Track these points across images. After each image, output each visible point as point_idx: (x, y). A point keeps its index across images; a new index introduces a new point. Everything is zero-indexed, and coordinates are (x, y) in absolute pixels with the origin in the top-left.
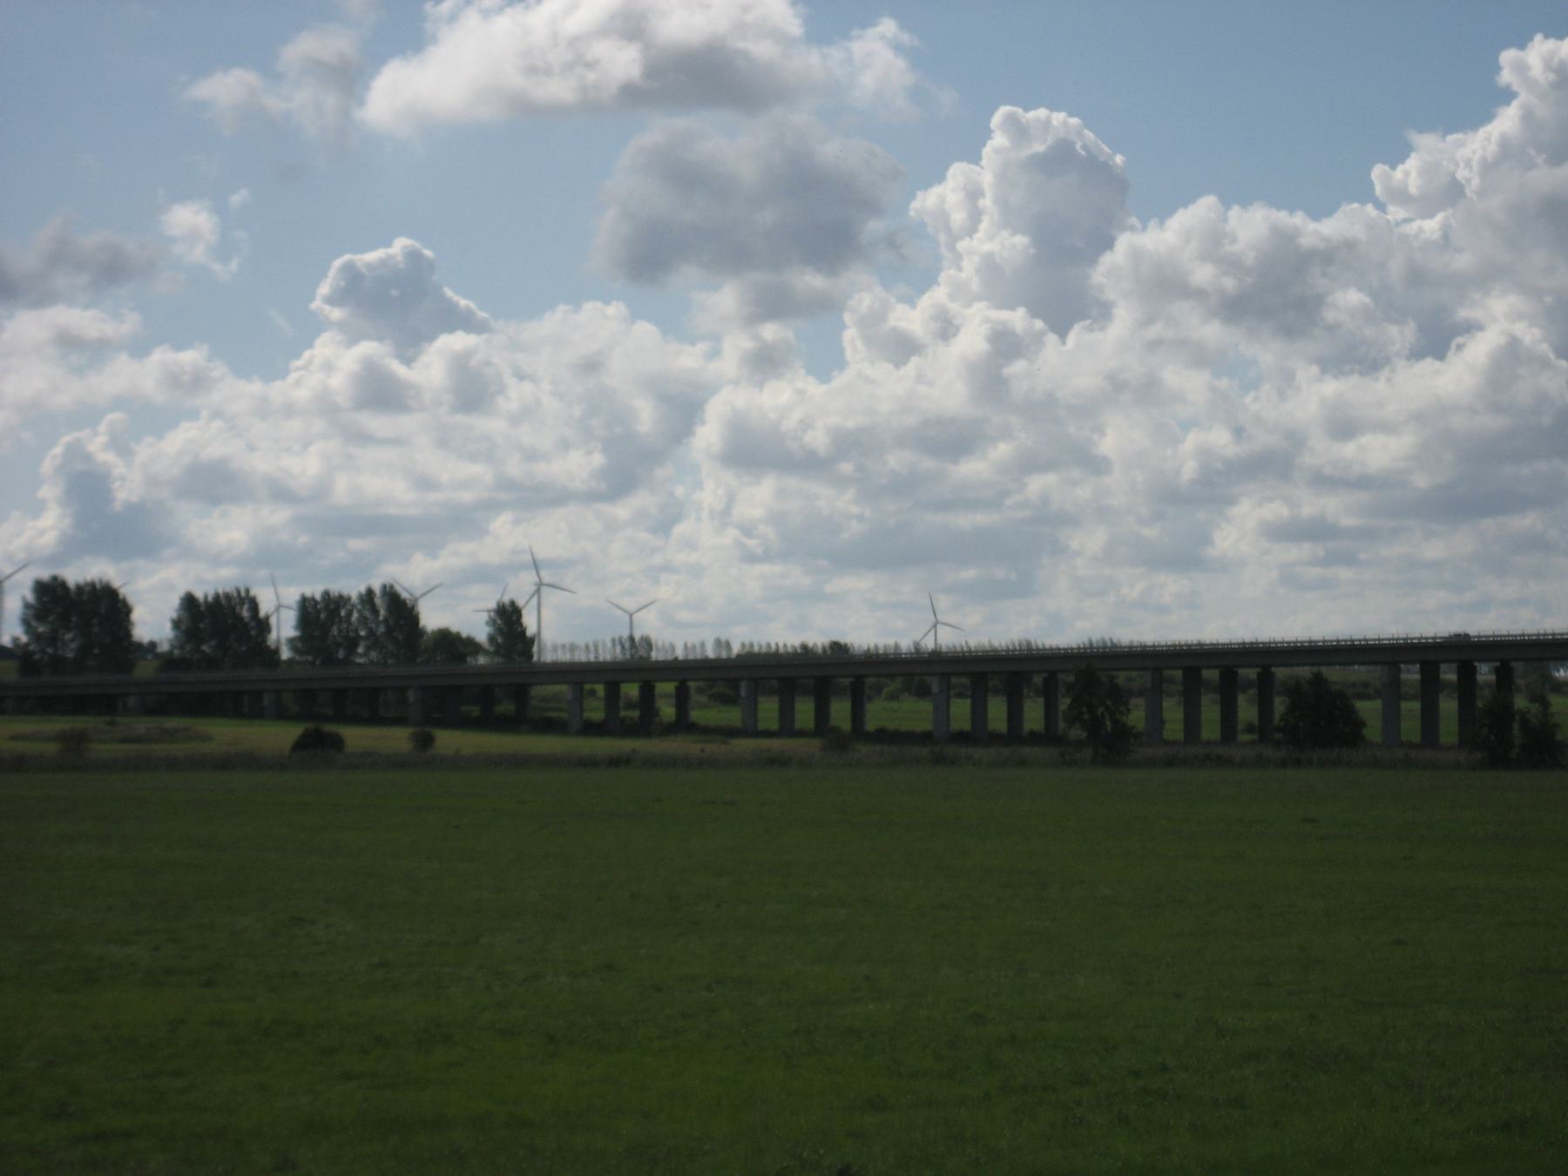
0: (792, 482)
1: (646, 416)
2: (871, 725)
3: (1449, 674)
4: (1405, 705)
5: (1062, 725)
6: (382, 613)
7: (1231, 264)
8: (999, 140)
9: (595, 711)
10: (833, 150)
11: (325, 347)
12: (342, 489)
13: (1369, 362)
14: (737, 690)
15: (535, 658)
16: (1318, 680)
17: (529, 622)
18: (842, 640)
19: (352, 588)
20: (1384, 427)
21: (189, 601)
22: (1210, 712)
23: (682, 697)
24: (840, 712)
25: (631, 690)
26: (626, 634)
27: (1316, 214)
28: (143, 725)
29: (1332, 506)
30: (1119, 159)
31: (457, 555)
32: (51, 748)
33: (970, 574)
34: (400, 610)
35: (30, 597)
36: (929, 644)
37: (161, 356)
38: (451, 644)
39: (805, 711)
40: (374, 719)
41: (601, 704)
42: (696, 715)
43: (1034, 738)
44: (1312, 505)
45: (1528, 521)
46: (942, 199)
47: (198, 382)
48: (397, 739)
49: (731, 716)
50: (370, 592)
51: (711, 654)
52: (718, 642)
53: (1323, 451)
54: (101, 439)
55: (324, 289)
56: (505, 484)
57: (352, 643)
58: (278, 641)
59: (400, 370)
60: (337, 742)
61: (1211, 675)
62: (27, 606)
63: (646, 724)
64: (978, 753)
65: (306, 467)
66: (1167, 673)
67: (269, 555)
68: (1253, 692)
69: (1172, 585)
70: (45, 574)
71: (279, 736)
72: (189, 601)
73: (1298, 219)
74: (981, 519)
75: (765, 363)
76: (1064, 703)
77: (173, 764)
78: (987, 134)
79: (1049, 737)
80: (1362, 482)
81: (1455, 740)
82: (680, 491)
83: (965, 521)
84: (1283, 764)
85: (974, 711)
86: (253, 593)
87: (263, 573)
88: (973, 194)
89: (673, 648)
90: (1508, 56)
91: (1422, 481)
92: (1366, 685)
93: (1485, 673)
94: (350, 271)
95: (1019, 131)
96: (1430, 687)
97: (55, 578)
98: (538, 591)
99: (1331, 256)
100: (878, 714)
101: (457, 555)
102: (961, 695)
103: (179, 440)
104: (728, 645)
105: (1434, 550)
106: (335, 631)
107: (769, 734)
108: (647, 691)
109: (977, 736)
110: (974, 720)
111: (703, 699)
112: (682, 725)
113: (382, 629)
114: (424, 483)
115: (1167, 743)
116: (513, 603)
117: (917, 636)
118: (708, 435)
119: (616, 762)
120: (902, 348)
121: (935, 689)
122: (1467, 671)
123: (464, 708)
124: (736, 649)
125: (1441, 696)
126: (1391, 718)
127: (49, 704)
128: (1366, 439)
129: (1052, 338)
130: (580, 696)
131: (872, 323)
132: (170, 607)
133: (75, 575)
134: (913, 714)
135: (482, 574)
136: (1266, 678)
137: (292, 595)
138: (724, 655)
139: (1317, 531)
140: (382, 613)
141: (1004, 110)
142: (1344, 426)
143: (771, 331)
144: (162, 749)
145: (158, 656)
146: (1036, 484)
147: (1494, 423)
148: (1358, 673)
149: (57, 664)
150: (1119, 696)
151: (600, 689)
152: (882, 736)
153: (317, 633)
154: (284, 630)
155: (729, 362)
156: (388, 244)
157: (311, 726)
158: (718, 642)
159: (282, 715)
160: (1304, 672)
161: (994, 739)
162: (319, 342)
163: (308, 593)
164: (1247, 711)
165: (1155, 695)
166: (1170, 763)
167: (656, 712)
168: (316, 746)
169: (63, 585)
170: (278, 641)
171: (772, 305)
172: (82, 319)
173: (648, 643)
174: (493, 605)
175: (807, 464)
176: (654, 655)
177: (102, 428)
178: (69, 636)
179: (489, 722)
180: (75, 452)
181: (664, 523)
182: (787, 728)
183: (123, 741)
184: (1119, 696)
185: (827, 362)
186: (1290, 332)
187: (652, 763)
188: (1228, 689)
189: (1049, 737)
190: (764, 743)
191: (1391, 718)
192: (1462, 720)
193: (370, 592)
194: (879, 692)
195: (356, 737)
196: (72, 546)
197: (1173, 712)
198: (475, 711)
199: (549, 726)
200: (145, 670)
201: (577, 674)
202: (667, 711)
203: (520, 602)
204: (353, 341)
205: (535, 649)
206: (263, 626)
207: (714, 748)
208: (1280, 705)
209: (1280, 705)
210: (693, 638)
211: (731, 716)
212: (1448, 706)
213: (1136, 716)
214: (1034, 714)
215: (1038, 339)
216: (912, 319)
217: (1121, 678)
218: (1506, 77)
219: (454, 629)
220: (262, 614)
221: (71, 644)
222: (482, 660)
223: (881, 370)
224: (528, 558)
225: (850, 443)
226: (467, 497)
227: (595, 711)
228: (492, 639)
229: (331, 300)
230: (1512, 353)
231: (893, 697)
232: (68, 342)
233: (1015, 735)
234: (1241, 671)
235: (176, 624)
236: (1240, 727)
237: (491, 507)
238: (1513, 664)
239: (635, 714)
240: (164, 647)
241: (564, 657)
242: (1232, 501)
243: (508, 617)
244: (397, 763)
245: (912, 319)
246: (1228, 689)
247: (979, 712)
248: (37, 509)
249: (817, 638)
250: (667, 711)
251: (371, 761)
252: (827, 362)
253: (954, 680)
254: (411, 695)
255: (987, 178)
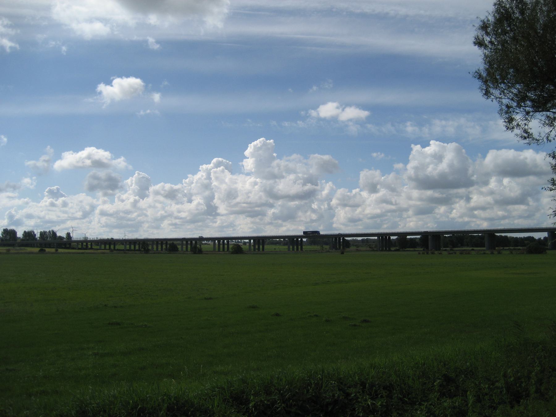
0: (109, 218)
1: (88, 208)
2: (116, 249)
3: (189, 242)
4: (184, 246)
5: (141, 248)
6: (51, 233)
7: (165, 190)
8: (136, 174)
9: (80, 247)
10: (114, 175)
11: (45, 199)
12: (47, 217)
13: (182, 203)
14: (99, 244)
15: (72, 240)
16: (173, 243)
17: (71, 235)
18: (113, 238)
19: (47, 230)
20: (185, 212)
21: (25, 232)
22: (160, 247)
23: (91, 245)
24: (112, 247)
25: (85, 244)
26: (84, 237)
27: (176, 185)
28: (18, 248)
29: (177, 221)
30: (149, 177)
31: (62, 226)
32: (5, 251)
33: (130, 229)
34: (54, 234)
35: (3, 231)
36: (124, 238)
37: (22, 199)
38: (61, 238)
39: (107, 247)
40: (50, 247)
41: (81, 246)
42: (93, 247)
43: (137, 250)
44: (175, 221)
45: (200, 224)
46: (128, 181)
47: (27, 203)
48: (53, 250)
49: (98, 247)
50: (50, 231)
51: (96, 239)
52: (96, 238)
53: (176, 214)
54: (13, 210)
55: (47, 190)
56: (69, 217)
57: (47, 238)
58: (37, 237)
59: (56, 202)
60: (45, 250)
61: (160, 242)
62: (2, 232)
63: (87, 248)
64: (130, 252)
65: (42, 214)
66: (154, 242)
67: (37, 226)
68: (165, 244)
69: (155, 231)
70: (5, 228)
71: (37, 250)
72: (25, 232)
73: (173, 186)
74: (132, 222)
75: (104, 202)
76: (141, 246)
77: (22, 253)
78: (135, 174)
79: (139, 250)
80: (181, 218)
81: (190, 250)
82: (92, 218)
83: (130, 223)
84: (168, 253)
85: (109, 247)
86: (34, 231)
87: (35, 228)
88: (132, 181)
89: (91, 238)
90: (201, 166)
91: (188, 218)
92: (179, 244)
93: (194, 242)
94: (50, 189)
95: (139, 174)
96: (187, 244)
97: (6, 229)
98: (73, 231)
99: (177, 191)
100: (117, 247)
101: (62, 226)
102: (128, 245)
103: (24, 211)
104: (98, 238)
105: (189, 227)
106: (45, 236)
107: (103, 250)
108: (87, 244)
109: (130, 250)
110: (129, 248)
111: (94, 245)
112: (91, 248)
113: (51, 236)
114: (59, 217)
115: (154, 251)
116: (69, 233)
117: (122, 237)
118: (97, 211)
119: (83, 253)
120: (123, 201)
121: (125, 244)
122: (191, 242)
123: (62, 246)
124: (99, 239)
125: (188, 245)
126: (182, 247)
127: (4, 245)
128: (182, 213)
129: (141, 200)
130: (78, 244)
131: (119, 198)
132: (22, 233)
133: (9, 228)
134: (122, 247)
135: (66, 229)
136: (167, 243)
137: (39, 231)
138: (97, 239)
139: (175, 224)
140: (51, 233)
141: (137, 172)
142: (179, 211)
143: (106, 198)
144: (20, 251)
145: (21, 239)
146: (139, 218)
147: (196, 212)
148: (178, 242)
149: (6, 240)
150: (148, 245)
151: (81, 244)
152: (118, 250)
153: (43, 236)
154: (38, 236)
155: (100, 202)
156: (54, 187)
157: (41, 248)
158: (96, 238)
159: (37, 247)
160: (171, 242)
161: (132, 250)
162: (44, 198)
163: (41, 231)
164: (164, 247)
165: (153, 245)
166: (154, 253)
167: (88, 247)
168: (42, 251)
169: (8, 230)
170: (421, 199)
171: (105, 195)
172: (11, 194)
173: (87, 238)
174: (67, 233)
175: (111, 215)
176: (88, 239)
177: (14, 209)
178: (8, 236)
179: (66, 248)
180: (10, 213)
181: (90, 222)
182: (105, 249)
183: (15, 250)
184: (148, 245)
185: (112, 202)
186: (172, 200)
187: (87, 253)
188: (162, 244)
189: (139, 250)
190: (102, 251)
191: (182, 247)
192: (191, 248)
193: (50, 231)
194: (117, 244)
195: (47, 250)
196: (9, 225)
197: (155, 247)
198: (64, 246)
199: (73, 248)
200: (19, 241)
201: (78, 242)
202: (89, 247)
203: (70, 233)
204: (49, 198)
205: (72, 239)
206: (35, 235)
207: (95, 251)
208: (168, 246)
209: (168, 246)
210: (93, 237)
211: (98, 247)
212: (189, 246)
213: (150, 248)
214: (137, 247)
215: (139, 200)
216: (124, 197)
217: (148, 243)
218: (200, 169)
219: (61, 236)
220: (35, 233)
221: (8, 237)
222: (65, 240)
223: (120, 203)
224: (71, 227)
225: (117, 212)
226: (63, 219)
227: (80, 247)
228: (66, 237)
229: (47, 192)
230: (199, 204)
231: (119, 245)
232: (9, 197)
233: (135, 250)
234: (88, 243)
235: (23, 235)
236: (84, 245)
237: (67, 220)
238: (197, 241)
239: (85, 247)
240: (21, 238)
241: (76, 239)
242: (164, 220)
243: (68, 234)
244: (53, 253)
245: (124, 197)
246: (162, 244)
247: (130, 247)
248: (4, 219)
249: (110, 237)
250: (89, 247)
251: (49, 253)
252: (112, 202)
253: (127, 243)
254: (55, 244)
255: (134, 179)
